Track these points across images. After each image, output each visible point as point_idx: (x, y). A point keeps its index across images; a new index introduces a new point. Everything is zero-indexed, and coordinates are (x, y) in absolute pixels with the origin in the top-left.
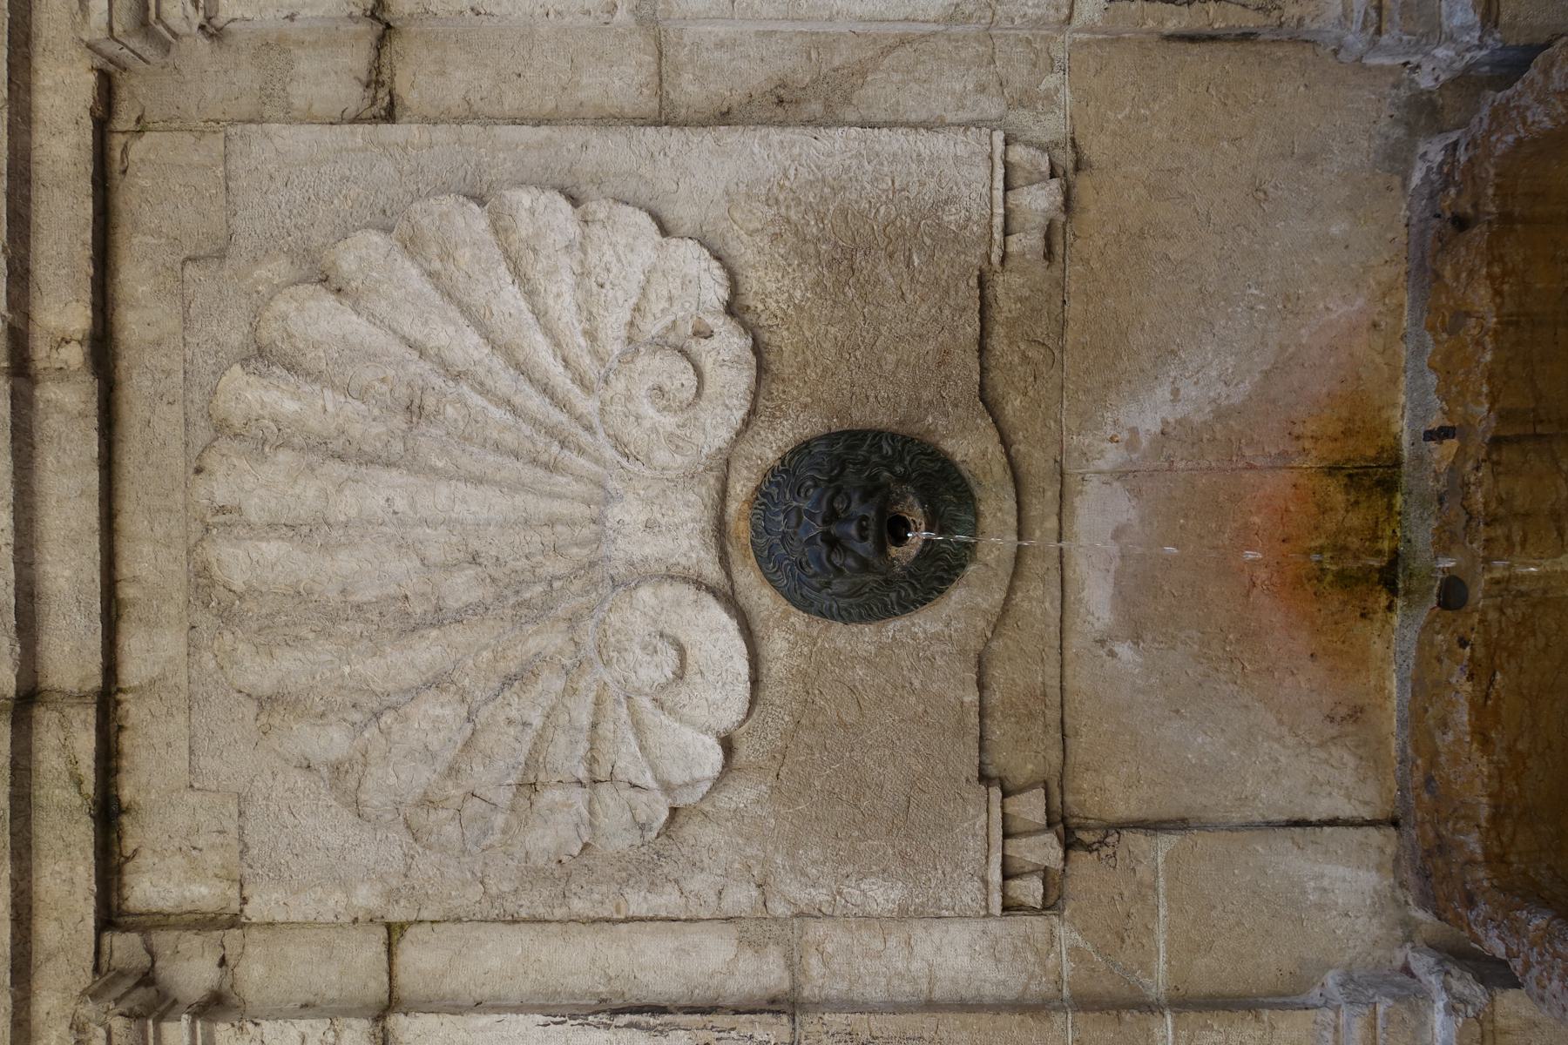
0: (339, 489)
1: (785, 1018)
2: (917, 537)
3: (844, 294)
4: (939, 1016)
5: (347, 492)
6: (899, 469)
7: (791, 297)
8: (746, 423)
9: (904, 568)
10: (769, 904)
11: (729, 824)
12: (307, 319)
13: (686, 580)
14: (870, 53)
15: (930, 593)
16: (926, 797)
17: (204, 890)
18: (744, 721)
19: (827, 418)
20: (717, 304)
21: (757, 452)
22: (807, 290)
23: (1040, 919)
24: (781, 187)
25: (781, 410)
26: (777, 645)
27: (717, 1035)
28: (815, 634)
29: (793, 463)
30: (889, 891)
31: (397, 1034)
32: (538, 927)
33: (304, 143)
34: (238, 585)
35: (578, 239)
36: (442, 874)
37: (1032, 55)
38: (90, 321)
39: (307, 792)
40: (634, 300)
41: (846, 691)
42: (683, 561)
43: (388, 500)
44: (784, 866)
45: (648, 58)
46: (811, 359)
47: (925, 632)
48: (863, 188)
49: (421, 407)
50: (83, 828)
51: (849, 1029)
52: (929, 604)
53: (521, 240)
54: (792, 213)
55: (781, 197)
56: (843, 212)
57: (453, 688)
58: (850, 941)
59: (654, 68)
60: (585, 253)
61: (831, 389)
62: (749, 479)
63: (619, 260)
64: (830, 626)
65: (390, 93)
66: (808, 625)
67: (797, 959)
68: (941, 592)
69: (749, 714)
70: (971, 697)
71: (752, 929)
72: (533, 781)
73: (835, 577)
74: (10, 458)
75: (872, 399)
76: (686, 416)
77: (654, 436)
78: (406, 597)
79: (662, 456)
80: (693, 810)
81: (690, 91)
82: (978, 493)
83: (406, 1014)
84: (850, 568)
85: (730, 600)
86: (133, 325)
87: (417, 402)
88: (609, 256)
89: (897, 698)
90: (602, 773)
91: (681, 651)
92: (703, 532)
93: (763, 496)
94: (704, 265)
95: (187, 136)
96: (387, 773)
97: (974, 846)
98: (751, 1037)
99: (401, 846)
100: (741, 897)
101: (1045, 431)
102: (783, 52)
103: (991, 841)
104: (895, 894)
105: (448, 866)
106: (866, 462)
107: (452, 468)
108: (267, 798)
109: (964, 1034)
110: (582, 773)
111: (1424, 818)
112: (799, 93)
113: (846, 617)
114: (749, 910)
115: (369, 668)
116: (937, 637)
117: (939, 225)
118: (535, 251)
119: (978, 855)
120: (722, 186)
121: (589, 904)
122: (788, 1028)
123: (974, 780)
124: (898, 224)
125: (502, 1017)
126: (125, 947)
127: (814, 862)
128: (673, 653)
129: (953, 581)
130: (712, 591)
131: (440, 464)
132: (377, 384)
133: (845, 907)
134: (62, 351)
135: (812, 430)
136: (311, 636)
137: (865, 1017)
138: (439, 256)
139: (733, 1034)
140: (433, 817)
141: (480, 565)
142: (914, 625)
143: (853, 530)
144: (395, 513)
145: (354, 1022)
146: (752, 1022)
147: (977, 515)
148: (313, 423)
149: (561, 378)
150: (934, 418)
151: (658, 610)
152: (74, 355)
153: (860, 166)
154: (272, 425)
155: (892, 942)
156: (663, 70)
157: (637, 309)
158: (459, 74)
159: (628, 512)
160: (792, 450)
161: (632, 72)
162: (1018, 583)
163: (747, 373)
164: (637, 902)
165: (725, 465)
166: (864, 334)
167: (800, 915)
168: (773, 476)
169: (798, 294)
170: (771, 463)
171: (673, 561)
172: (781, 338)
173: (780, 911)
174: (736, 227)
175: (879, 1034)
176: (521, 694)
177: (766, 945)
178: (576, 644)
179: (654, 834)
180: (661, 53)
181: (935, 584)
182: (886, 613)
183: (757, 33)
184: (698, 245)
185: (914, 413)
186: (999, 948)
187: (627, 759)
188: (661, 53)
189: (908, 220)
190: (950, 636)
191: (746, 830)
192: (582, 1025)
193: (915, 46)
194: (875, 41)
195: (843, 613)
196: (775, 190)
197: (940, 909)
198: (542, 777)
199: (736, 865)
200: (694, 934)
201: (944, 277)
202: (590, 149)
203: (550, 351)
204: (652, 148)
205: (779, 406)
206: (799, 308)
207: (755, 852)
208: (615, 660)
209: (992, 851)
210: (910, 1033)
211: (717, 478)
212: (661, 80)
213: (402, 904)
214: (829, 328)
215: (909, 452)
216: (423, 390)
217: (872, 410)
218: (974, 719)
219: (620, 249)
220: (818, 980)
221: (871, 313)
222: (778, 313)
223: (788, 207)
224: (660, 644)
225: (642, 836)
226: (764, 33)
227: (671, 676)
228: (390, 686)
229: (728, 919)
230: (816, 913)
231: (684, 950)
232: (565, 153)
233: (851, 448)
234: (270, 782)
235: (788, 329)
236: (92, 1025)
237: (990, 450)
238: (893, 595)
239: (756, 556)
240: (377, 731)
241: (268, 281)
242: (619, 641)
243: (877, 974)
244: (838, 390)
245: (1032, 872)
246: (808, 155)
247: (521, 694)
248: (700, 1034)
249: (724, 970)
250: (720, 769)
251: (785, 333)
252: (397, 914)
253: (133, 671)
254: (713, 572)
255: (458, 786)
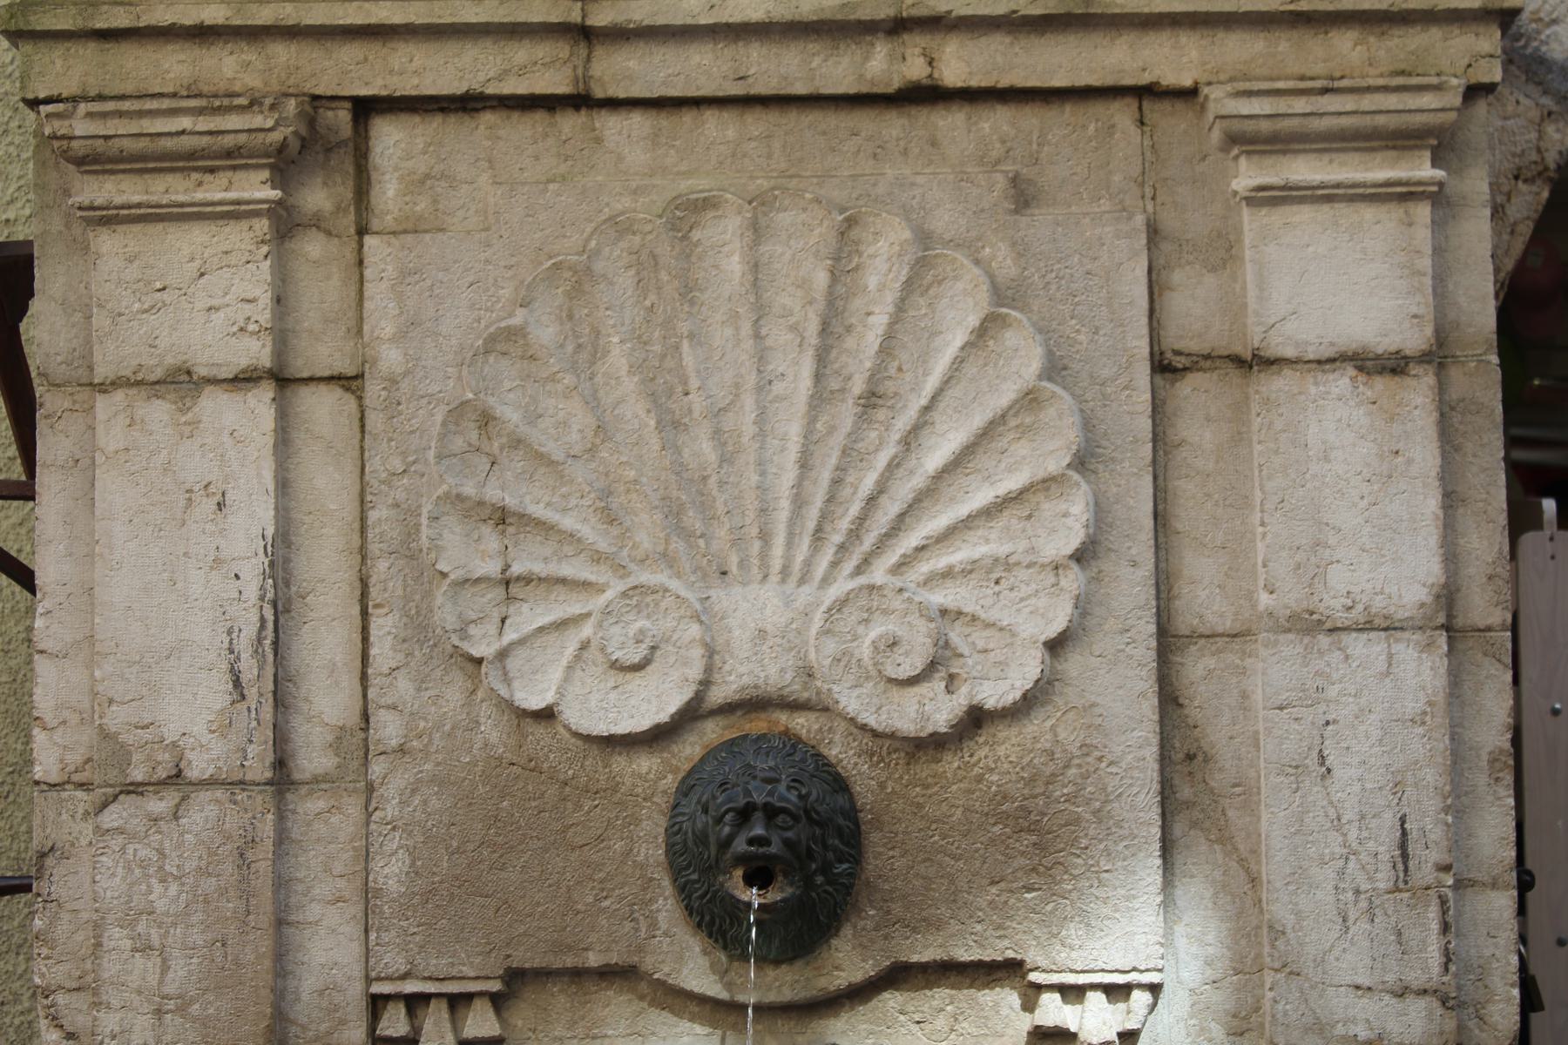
0: (793, 328)
1: (269, 774)
2: (753, 896)
3: (994, 824)
4: (271, 931)
5: (790, 336)
6: (819, 879)
7: (992, 770)
8: (864, 728)
9: (722, 885)
10: (382, 757)
11: (464, 716)
12: (956, 299)
13: (709, 669)
14: (1241, 847)
15: (698, 913)
16: (491, 913)
17: (391, 193)
18: (570, 730)
19: (872, 808)
20: (980, 697)
21: (837, 738)
22: (998, 786)
23: (364, 1036)
24: (1100, 759)
25: (878, 763)
26: (645, 763)
27: (253, 707)
28: (655, 799)
29: (825, 775)
30: (396, 879)
31: (255, 391)
32: (357, 525)
33: (1130, 290)
34: (696, 235)
35: (1041, 560)
36: (412, 432)
37: (1244, 1013)
38: (951, 86)
39: (494, 299)
40: (983, 616)
41: (599, 832)
42: (727, 667)
43: (783, 375)
44: (421, 772)
45: (1228, 624)
46: (929, 792)
47: (658, 911)
48: (1101, 841)
49: (874, 406)
50: (456, 84)
51: (257, 839)
52: (686, 913)
53: (1038, 503)
54: (1073, 771)
55: (1089, 759)
56: (1076, 821)
57: (598, 441)
58: (342, 840)
59: (1220, 629)
60: (1028, 566)
61: (901, 811)
62: (809, 731)
63: (1022, 600)
64: (664, 815)
65: (1185, 369)
66: (665, 792)
67: (324, 786)
68: (699, 925)
69: (577, 735)
70: (593, 960)
71: (354, 740)
72: (507, 521)
73: (713, 817)
74: (815, 18)
75: (891, 853)
76: (870, 668)
77: (849, 637)
78: (687, 394)
79: (831, 646)
80: (476, 679)
81: (1197, 667)
82: (799, 964)
83: (274, 399)
84: (721, 829)
85: (690, 715)
86: (950, 122)
87: (880, 402)
88: (1025, 590)
89: (591, 884)
90: (515, 589)
91: (638, 667)
92: (756, 687)
93: (793, 745)
94: (1018, 684)
95: (1139, 169)
96: (514, 380)
97: (438, 965)
98: (251, 741)
99: (440, 392)
100: (388, 729)
101: (864, 1034)
102: (1239, 759)
103: (446, 982)
104: (392, 884)
105: (421, 437)
106: (825, 847)
107: (815, 437)
108: (487, 261)
109: (252, 957)
110: (517, 569)
111: (861, 608)
112: (1199, 776)
113: (673, 831)
114: (377, 737)
115: (618, 358)
116: (653, 925)
117: (1065, 918)
118: (1029, 517)
119: (433, 969)
120: (1098, 700)
121: (383, 577)
122: (259, 778)
123: (508, 963)
124: (1066, 877)
125: (272, 494)
126: (342, 117)
127: (425, 802)
128: (636, 659)
129: (710, 936)
130: (698, 697)
131: (819, 426)
132: (896, 364)
133: (380, 834)
134: (922, 59)
135: (859, 793)
136: (648, 303)
137: (270, 856)
138: (1022, 424)
139: (254, 724)
140: (472, 425)
141: (720, 466)
142: (666, 899)
143: (759, 831)
144: (770, 382)
145: (268, 350)
146: (266, 742)
147: (777, 962)
148: (857, 303)
149: (910, 540)
150: (873, 916)
151: (678, 644)
152: (915, 70)
153: (1122, 838)
154: (853, 265)
155: (341, 883)
156: (1218, 639)
157: (974, 618)
158: (1208, 435)
159: (774, 613)
160: (839, 774)
161: (1215, 608)
162: (708, 1007)
163: (912, 729)
164: (384, 626)
165: (823, 708)
166: (956, 844)
167: (370, 788)
168: (812, 755)
169: (995, 778)
170: (825, 752)
171: (727, 657)
172: (950, 763)
173: (376, 768)
174: (1059, 714)
175: (252, 870)
176: (592, 509)
177: (337, 755)
178: (642, 561)
179: (457, 643)
180: (1235, 636)
181: (707, 918)
182: (676, 870)
183: (1257, 732)
184: (1036, 678)
185: (878, 896)
186: (334, 994)
187: (530, 616)
188: (1235, 636)
189: (1070, 887)
190: (654, 937)
191: (459, 733)
192: (264, 573)
193: (1249, 893)
194: (1253, 852)
195: (677, 827)
196: (1097, 754)
197: (378, 931)
198: (511, 530)
199: (422, 724)
200: (350, 682)
201: (1014, 925)
202: (1132, 569)
203: (931, 533)
204: (1133, 631)
205: (883, 760)
206: (979, 779)
207: (436, 742)
208: (628, 602)
209: (437, 983)
210: (253, 901)
211: (809, 700)
212: (1208, 636)
213: (383, 393)
214: (961, 809)
215: (836, 890)
216: (892, 407)
217: (880, 854)
218: (570, 961)
219: (1033, 601)
220: (309, 806)
221: (977, 850)
222: (975, 758)
223: (1079, 766)
224: (644, 646)
225: (455, 631)
226: (1257, 740)
227: (614, 658)
228: (599, 379)
229: (366, 717)
230: (373, 805)
231: (333, 671)
232: (1127, 545)
233: (840, 832)
234: (502, 263)
235: (959, 768)
236: (276, 116)
237: (842, 974)
238: (695, 877)
239: (733, 740)
240: (555, 369)
241: (993, 257)
242: (648, 605)
243: (308, 868)
244: (899, 819)
245: (412, 1026)
246: (1131, 785)
247: (592, 509)
248: (254, 690)
249: (312, 713)
250: (523, 706)
251: (956, 765)
252: (374, 390)
253: (612, 125)
254: (717, 696)
255: (502, 449)
